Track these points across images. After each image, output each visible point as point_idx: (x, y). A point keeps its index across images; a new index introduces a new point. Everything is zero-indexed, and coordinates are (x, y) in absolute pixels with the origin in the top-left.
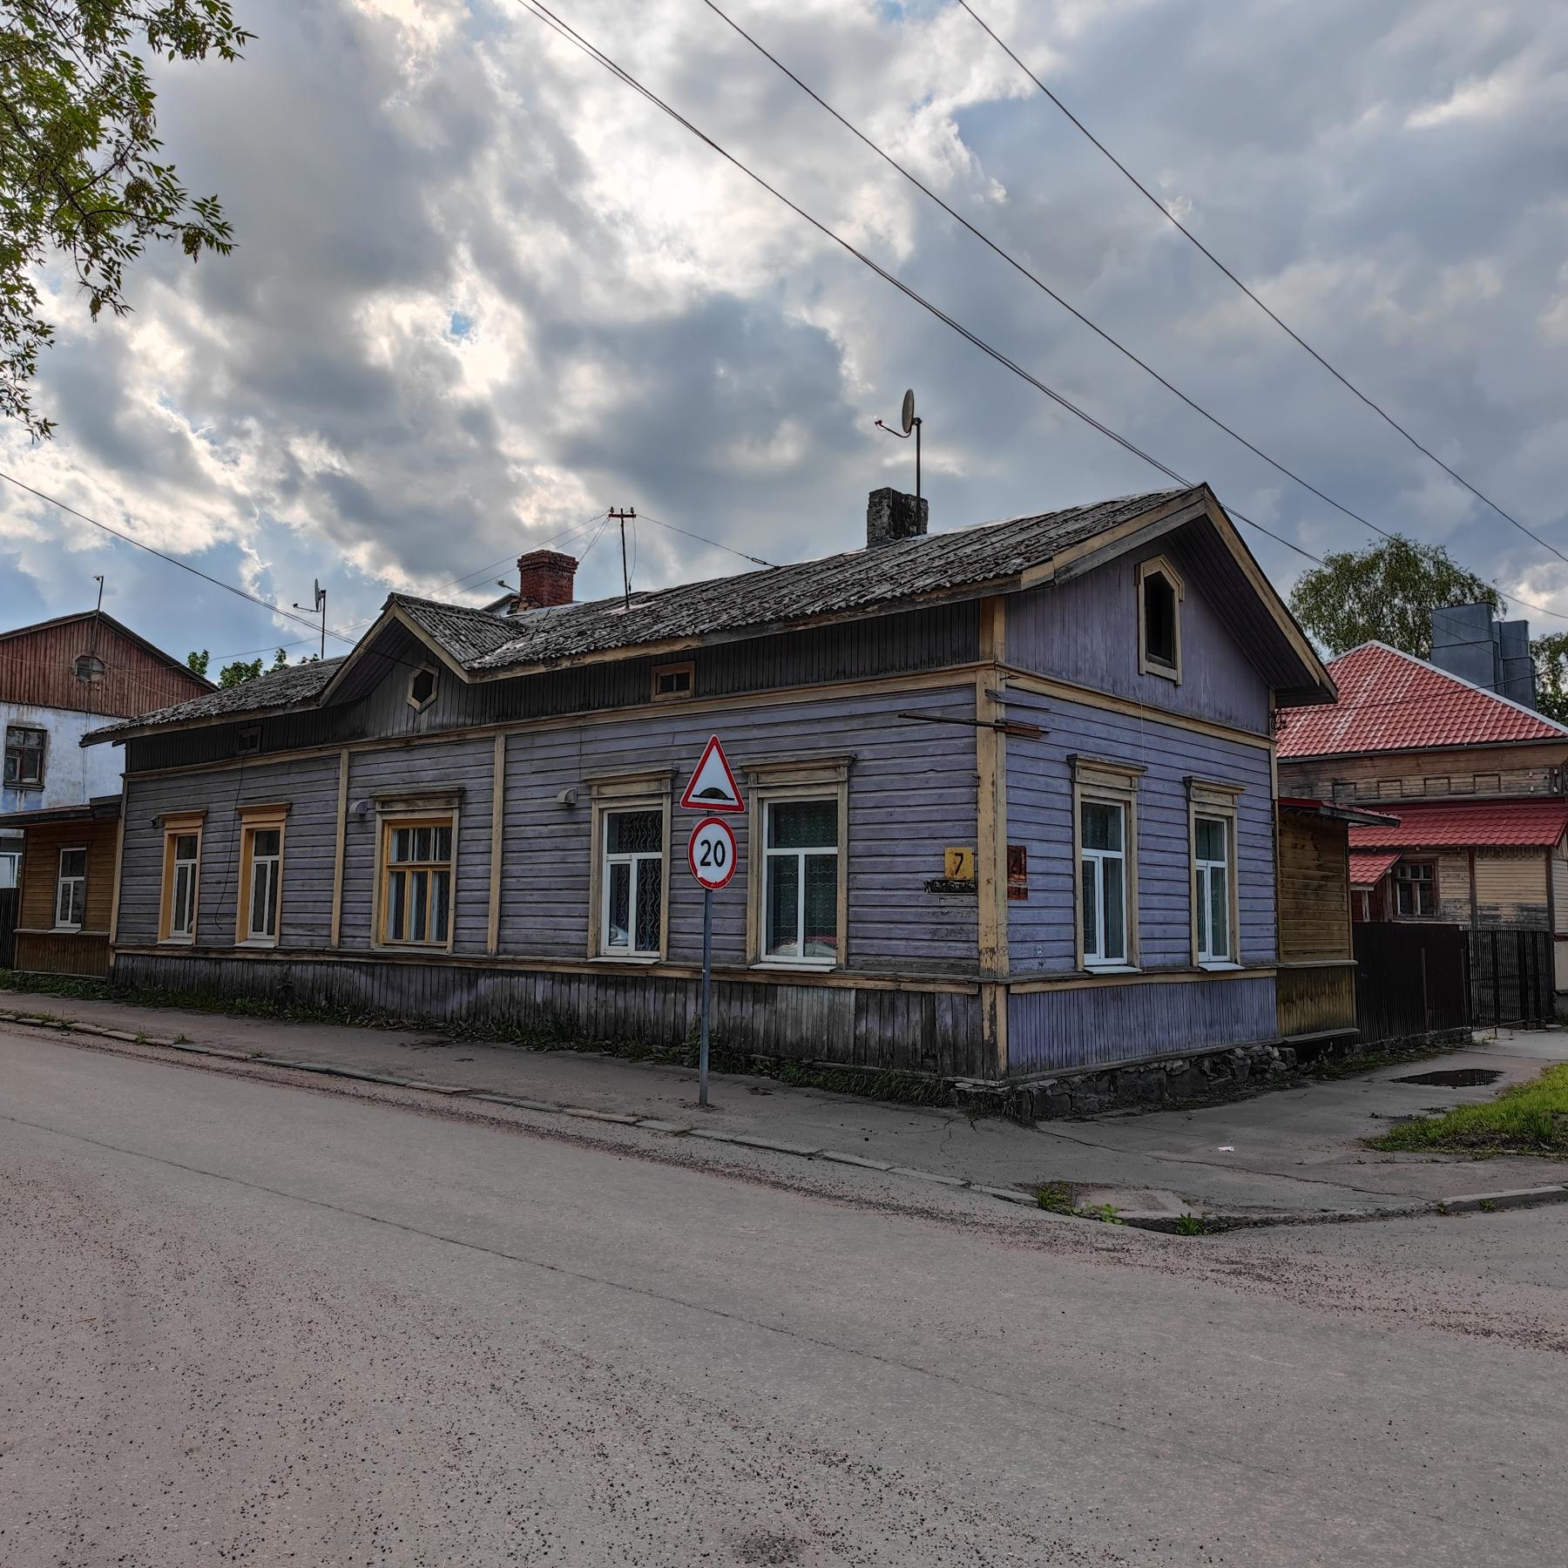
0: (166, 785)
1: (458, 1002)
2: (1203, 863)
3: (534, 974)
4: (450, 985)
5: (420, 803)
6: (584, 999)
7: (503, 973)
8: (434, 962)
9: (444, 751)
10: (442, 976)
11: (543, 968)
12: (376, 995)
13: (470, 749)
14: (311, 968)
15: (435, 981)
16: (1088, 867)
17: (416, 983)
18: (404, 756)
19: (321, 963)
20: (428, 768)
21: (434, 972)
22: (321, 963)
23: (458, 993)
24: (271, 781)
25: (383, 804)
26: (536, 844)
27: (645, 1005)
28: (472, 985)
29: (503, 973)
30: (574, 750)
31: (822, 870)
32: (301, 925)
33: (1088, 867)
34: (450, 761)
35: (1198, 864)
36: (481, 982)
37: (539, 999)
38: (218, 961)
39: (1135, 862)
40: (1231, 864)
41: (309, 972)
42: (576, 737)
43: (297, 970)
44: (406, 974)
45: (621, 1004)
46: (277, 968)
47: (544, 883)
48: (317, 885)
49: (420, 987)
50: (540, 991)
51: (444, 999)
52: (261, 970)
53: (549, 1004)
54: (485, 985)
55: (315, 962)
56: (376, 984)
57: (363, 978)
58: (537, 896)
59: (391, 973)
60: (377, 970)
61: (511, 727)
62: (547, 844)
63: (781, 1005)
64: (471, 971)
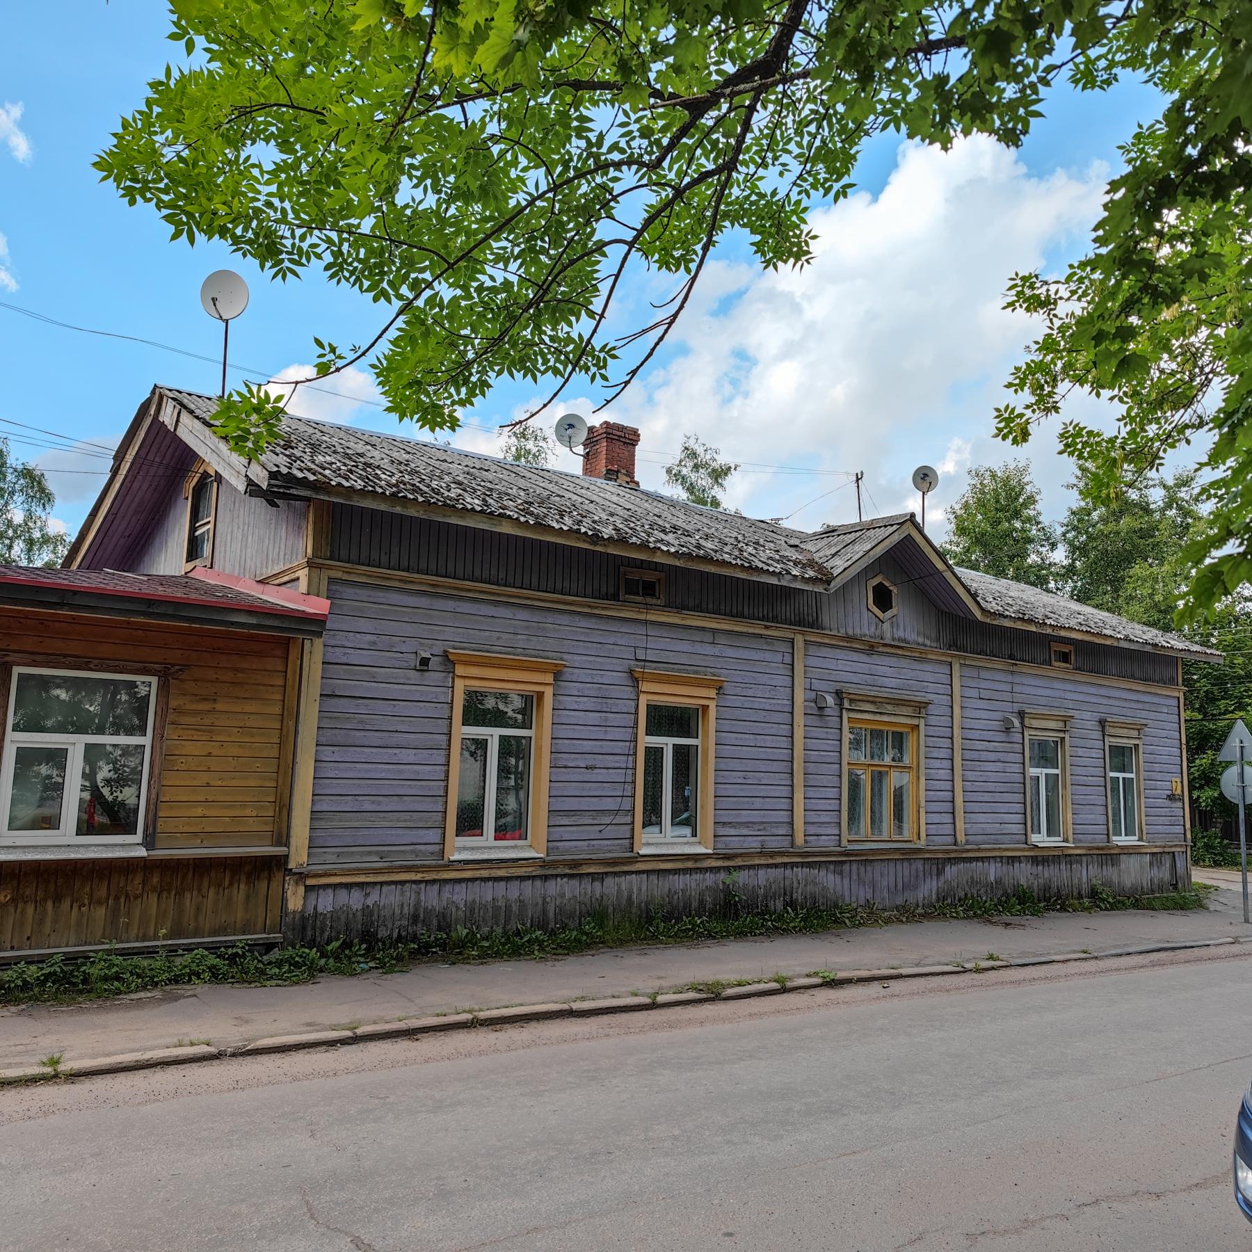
0: (440, 604)
1: (928, 889)
2: (1038, 770)
3: (988, 858)
4: (921, 874)
5: (889, 707)
6: (1024, 875)
7: (965, 860)
8: (909, 855)
9: (904, 663)
10: (914, 867)
11: (997, 854)
12: (847, 894)
13: (928, 667)
14: (761, 872)
15: (906, 873)
16: (482, 744)
17: (886, 876)
18: (864, 658)
19: (776, 866)
20: (890, 675)
21: (906, 864)
22: (776, 866)
23: (928, 881)
24: (685, 646)
25: (851, 701)
26: (984, 755)
27: (1057, 875)
28: (940, 873)
29: (965, 860)
30: (1008, 688)
31: (684, 758)
32: (746, 824)
33: (654, 755)
34: (910, 674)
35: (1033, 771)
36: (947, 868)
37: (992, 879)
38: (601, 877)
39: (1068, 774)
40: (1064, 770)
41: (763, 877)
42: (1009, 678)
43: (742, 877)
44: (869, 868)
45: (1046, 875)
46: (710, 879)
47: (991, 787)
48: (736, 777)
49: (892, 879)
50: (992, 872)
51: (916, 888)
52: (680, 882)
53: (999, 882)
54: (951, 872)
55: (768, 866)
56: (846, 882)
57: (831, 876)
58: (987, 797)
59: (862, 869)
60: (846, 867)
61: (965, 658)
62: (992, 756)
63: (1123, 866)
64: (939, 862)
